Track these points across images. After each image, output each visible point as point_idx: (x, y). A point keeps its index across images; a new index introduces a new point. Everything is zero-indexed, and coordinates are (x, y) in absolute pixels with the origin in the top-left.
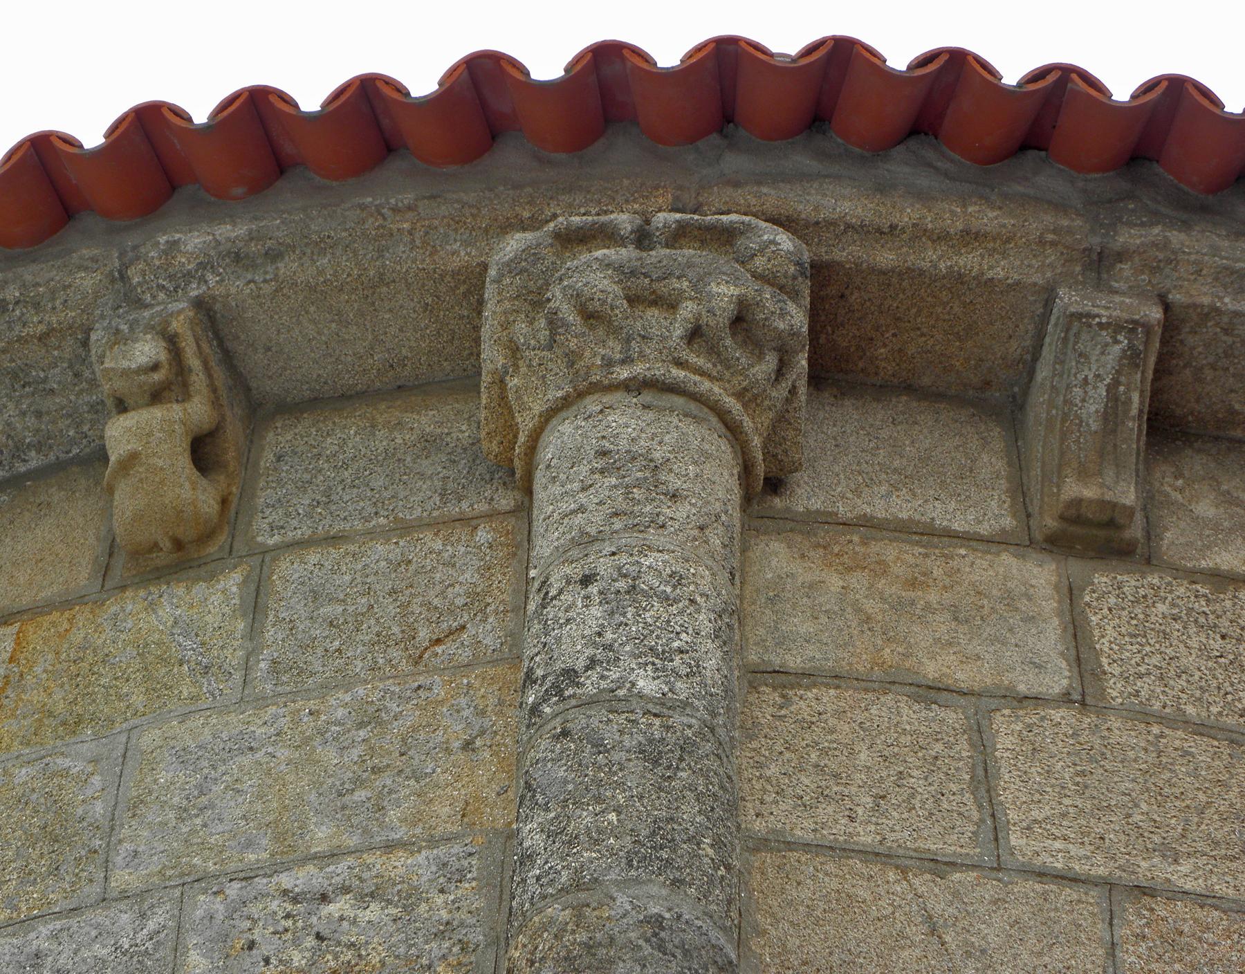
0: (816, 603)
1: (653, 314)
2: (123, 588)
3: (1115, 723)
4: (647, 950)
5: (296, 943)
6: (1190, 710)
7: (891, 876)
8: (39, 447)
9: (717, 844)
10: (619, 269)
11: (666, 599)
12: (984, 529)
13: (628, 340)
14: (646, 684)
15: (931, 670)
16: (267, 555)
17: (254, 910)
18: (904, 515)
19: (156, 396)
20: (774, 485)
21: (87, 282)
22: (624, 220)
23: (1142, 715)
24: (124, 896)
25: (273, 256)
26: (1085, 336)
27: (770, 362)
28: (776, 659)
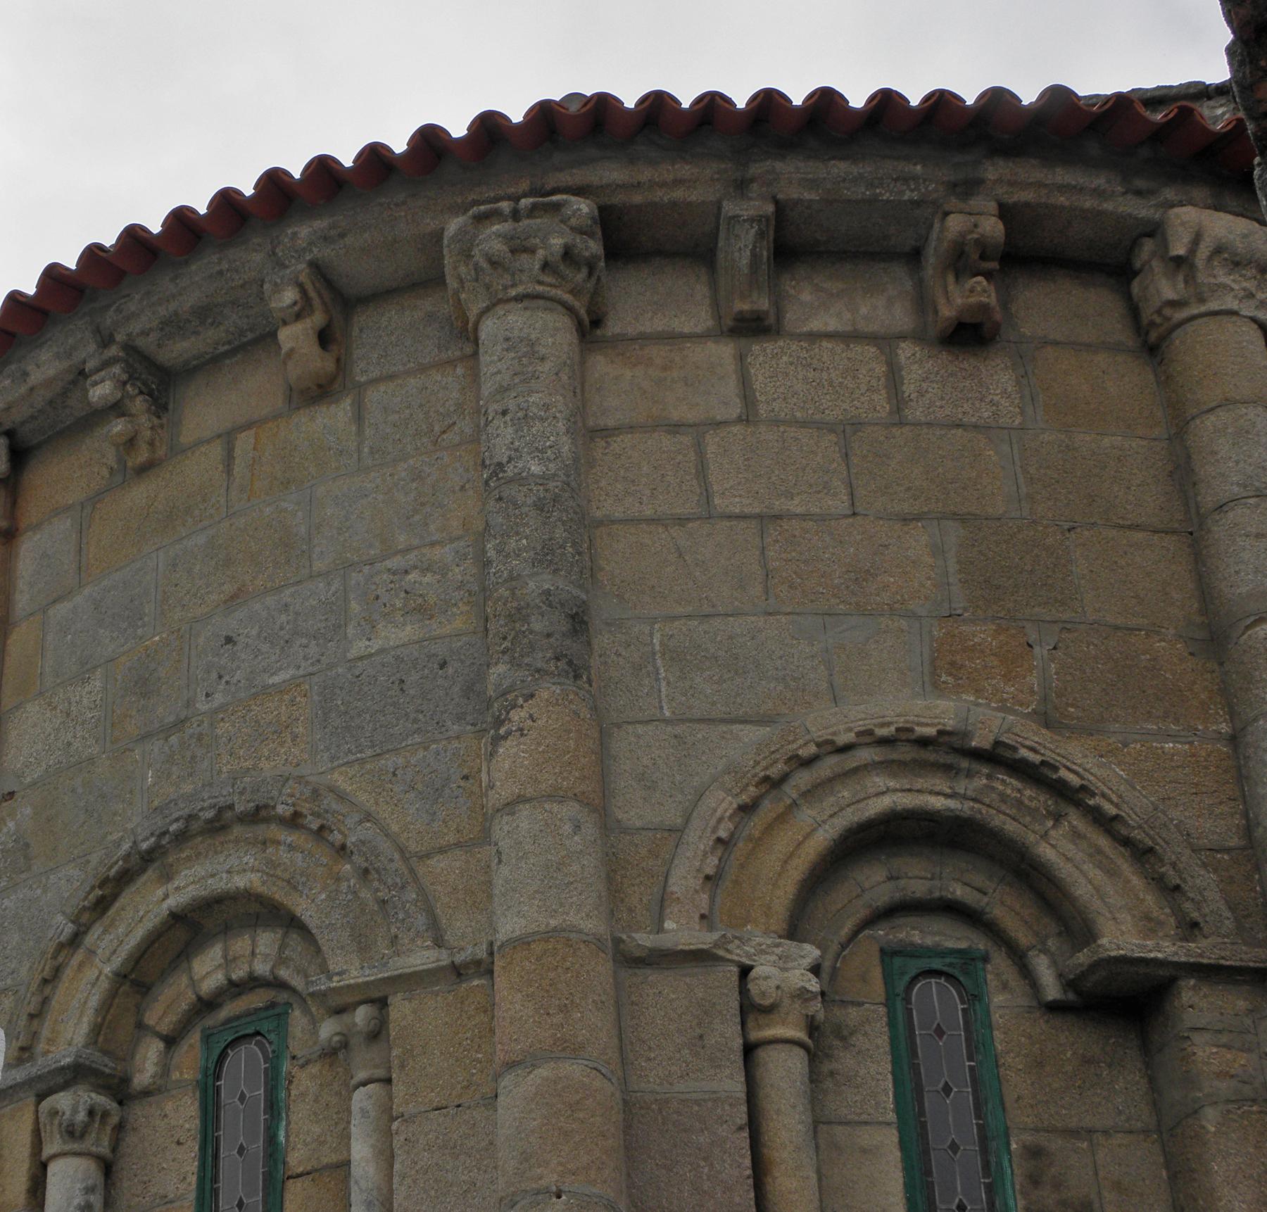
0: (619, 384)
1: (524, 256)
2: (299, 409)
3: (763, 428)
4: (544, 608)
5: (397, 596)
6: (798, 415)
7: (660, 530)
8: (251, 330)
9: (574, 544)
10: (505, 237)
11: (542, 419)
12: (699, 330)
13: (513, 275)
14: (535, 468)
15: (675, 416)
16: (361, 388)
17: (377, 580)
18: (660, 329)
19: (298, 317)
20: (597, 323)
21: (257, 257)
22: (505, 206)
23: (776, 422)
24: (319, 575)
25: (342, 236)
26: (737, 227)
27: (585, 271)
28: (602, 423)
